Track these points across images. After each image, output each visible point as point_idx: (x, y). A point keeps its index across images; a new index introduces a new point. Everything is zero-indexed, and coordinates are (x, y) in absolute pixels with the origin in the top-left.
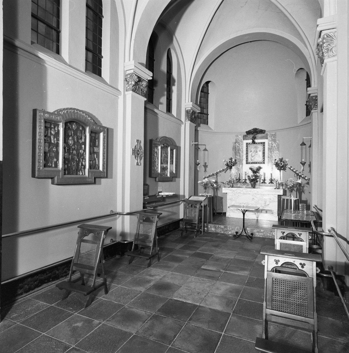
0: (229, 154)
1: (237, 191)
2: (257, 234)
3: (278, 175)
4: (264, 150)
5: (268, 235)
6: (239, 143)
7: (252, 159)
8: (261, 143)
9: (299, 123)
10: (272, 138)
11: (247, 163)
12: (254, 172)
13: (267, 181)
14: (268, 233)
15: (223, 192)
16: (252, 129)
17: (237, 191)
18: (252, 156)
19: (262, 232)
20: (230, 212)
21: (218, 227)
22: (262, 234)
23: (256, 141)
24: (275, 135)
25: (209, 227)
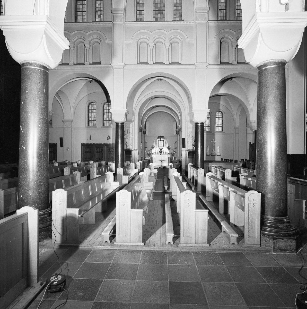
3: (168, 151)
12: (161, 150)
13: (165, 153)
23: (161, 140)
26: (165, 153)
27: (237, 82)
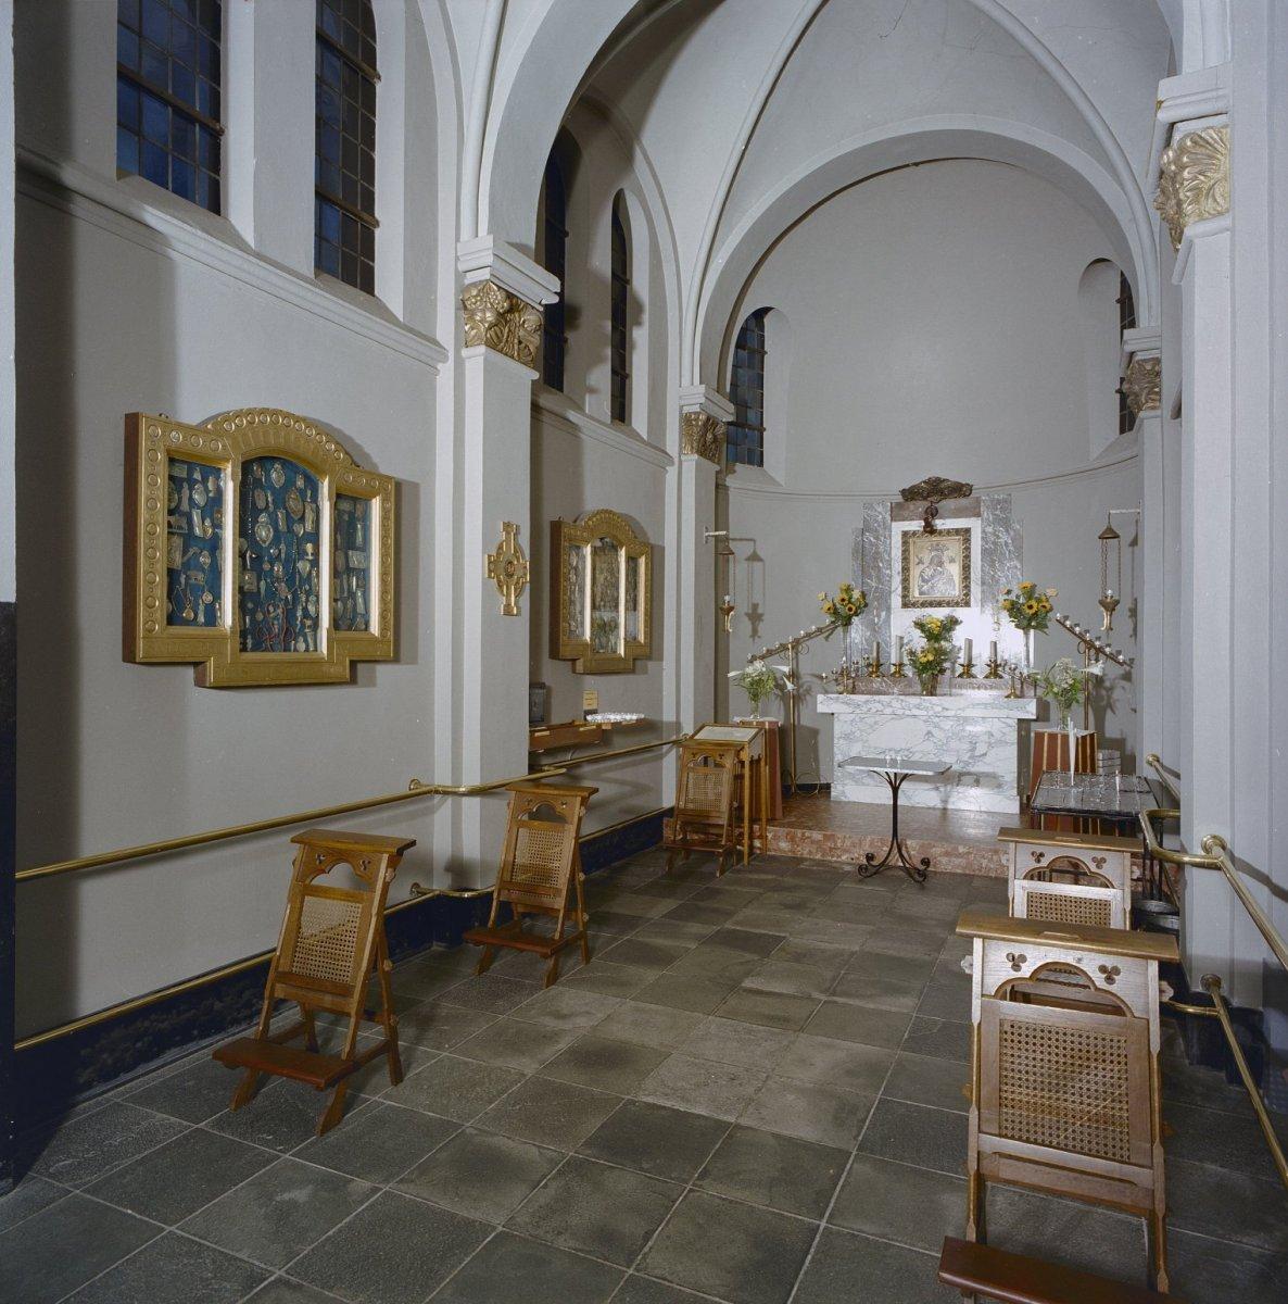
2: (944, 860)
3: (1015, 644)
4: (967, 557)
6: (876, 531)
8: (957, 531)
11: (905, 605)
13: (980, 670)
18: (923, 581)
19: (960, 855)
21: (803, 838)
22: (962, 861)
26: (980, 670)
27: (888, 1008)
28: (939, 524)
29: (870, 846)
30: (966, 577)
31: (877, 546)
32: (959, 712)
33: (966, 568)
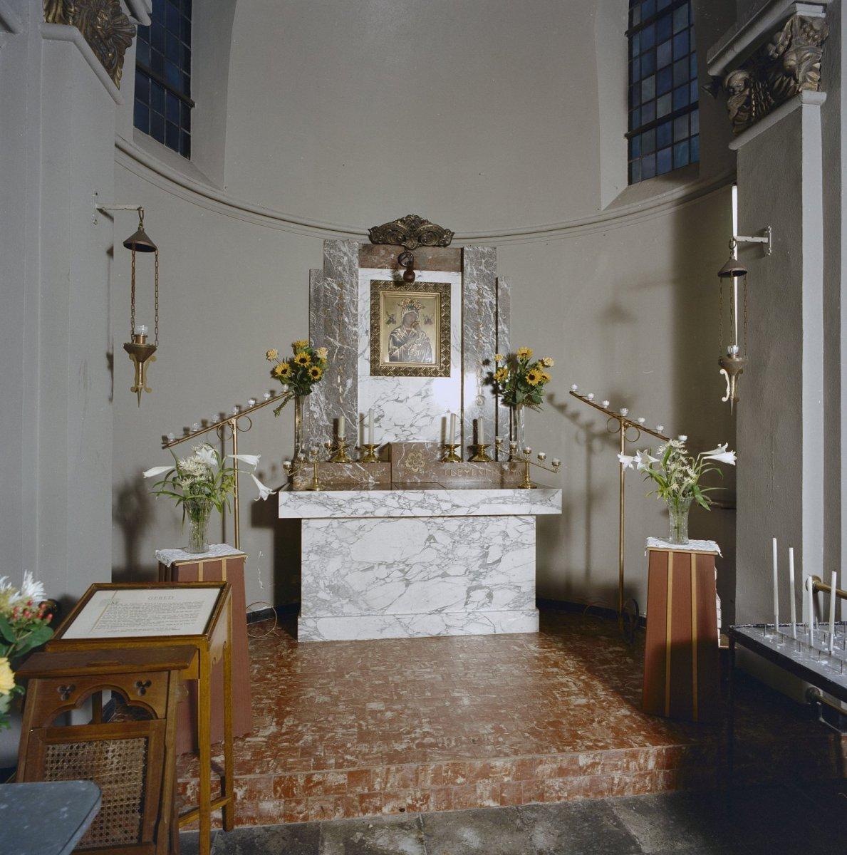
0: (290, 330)
1: (354, 507)
2: (557, 783)
5: (616, 781)
6: (341, 276)
7: (397, 352)
8: (436, 286)
9: (604, 206)
10: (482, 267)
11: (375, 372)
14: (616, 767)
15: (280, 517)
16: (401, 220)
17: (354, 507)
18: (395, 343)
19: (582, 771)
20: (318, 613)
21: (309, 785)
22: (583, 780)
24: (490, 255)
25: (240, 793)
28: (422, 276)
29: (434, 781)
30: (445, 342)
31: (341, 298)
32: (473, 509)
33: (445, 331)
